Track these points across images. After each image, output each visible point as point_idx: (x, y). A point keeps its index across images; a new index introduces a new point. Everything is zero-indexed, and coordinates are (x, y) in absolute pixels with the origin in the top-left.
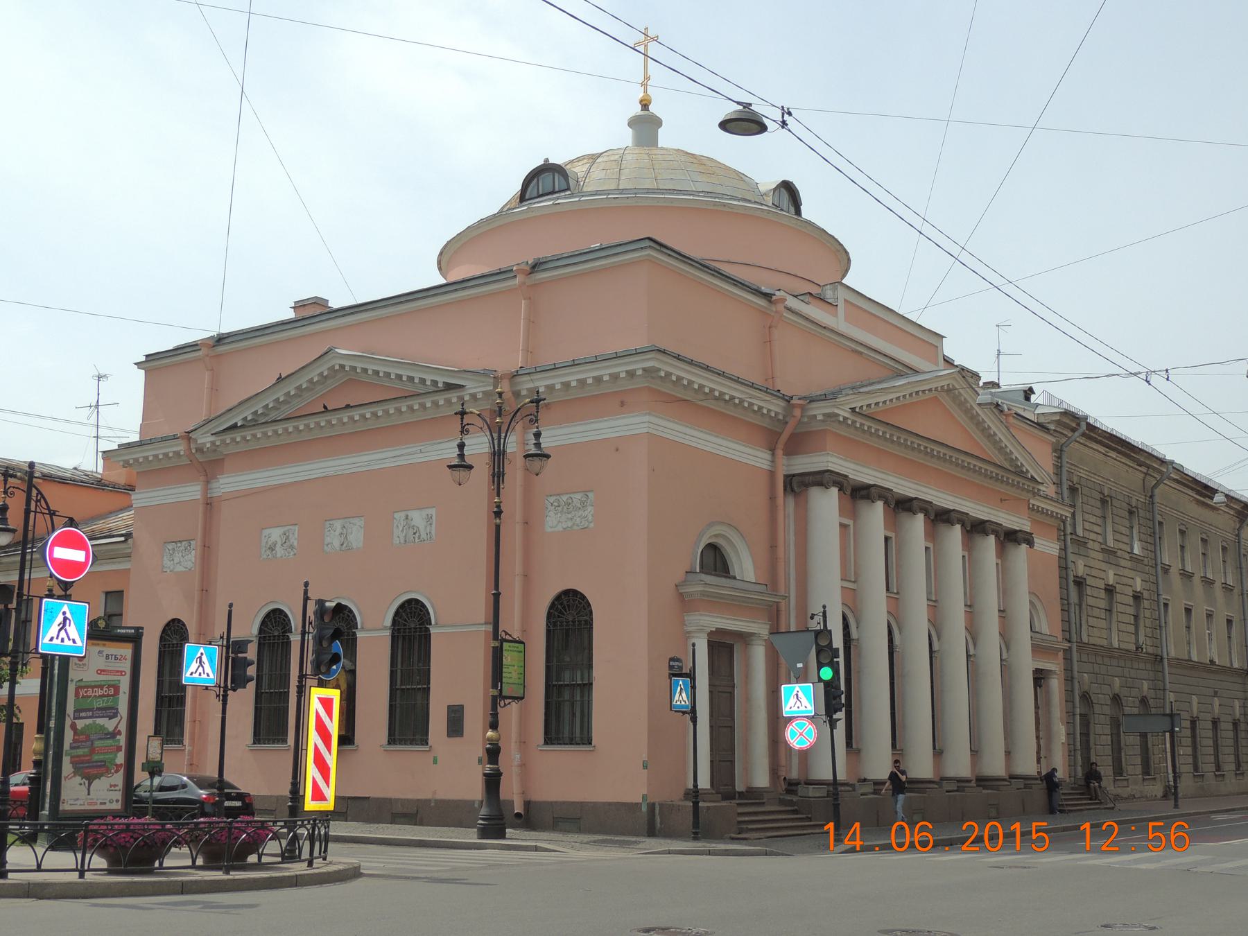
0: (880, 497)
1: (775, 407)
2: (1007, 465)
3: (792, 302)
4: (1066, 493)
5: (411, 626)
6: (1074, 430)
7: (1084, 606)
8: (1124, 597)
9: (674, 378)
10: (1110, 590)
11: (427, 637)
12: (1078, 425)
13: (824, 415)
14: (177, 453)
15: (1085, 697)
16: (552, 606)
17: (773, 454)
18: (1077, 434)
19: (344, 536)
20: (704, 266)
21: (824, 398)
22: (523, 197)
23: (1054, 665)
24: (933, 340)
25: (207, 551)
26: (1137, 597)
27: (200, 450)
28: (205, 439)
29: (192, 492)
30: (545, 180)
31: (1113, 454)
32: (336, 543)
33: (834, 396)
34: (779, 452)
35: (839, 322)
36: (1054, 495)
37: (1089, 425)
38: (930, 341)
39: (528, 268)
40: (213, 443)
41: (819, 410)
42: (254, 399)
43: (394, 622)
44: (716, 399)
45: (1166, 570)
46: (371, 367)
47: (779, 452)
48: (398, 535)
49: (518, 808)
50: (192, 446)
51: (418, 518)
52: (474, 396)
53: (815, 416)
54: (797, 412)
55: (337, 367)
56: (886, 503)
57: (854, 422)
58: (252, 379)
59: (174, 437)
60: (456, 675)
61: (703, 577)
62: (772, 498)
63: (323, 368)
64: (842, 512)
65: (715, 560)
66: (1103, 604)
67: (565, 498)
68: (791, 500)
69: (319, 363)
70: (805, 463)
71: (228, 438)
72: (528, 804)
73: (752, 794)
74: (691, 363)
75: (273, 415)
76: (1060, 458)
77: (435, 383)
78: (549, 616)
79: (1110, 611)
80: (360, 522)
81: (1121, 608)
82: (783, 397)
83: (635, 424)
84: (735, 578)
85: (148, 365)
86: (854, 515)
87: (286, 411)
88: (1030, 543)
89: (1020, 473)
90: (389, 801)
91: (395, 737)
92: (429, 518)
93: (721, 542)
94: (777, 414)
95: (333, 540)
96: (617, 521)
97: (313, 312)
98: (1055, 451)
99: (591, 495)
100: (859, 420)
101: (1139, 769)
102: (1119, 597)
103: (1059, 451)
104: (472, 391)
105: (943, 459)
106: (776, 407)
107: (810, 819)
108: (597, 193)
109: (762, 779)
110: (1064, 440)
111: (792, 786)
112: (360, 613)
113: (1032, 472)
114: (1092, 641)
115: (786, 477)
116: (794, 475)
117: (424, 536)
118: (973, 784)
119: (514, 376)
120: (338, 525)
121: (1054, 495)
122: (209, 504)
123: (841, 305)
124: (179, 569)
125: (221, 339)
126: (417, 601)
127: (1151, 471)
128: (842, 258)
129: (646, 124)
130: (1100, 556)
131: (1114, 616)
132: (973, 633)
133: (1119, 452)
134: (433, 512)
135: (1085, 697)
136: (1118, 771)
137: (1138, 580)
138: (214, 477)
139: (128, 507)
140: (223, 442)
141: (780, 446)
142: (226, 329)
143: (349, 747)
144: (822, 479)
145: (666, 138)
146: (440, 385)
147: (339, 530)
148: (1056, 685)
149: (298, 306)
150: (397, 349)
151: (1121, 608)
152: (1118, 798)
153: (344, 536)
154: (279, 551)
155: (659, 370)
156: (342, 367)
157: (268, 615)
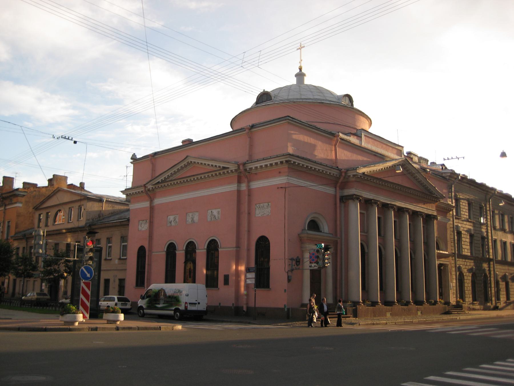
3: (341, 135)
5: (213, 247)
11: (175, 254)
17: (336, 189)
22: (257, 103)
25: (151, 223)
27: (149, 190)
28: (150, 187)
30: (264, 97)
31: (472, 187)
32: (190, 220)
34: (338, 188)
35: (365, 143)
40: (152, 188)
42: (163, 173)
43: (208, 247)
44: (313, 170)
47: (338, 188)
48: (209, 219)
49: (245, 309)
51: (215, 212)
52: (232, 171)
58: (162, 166)
59: (141, 186)
63: (185, 163)
65: (314, 225)
67: (261, 205)
70: (348, 192)
71: (157, 186)
75: (171, 178)
77: (219, 167)
78: (256, 245)
80: (197, 214)
83: (280, 180)
84: (321, 232)
86: (367, 210)
92: (218, 213)
93: (316, 220)
95: (189, 220)
96: (274, 214)
97: (188, 143)
99: (270, 204)
102: (475, 238)
117: (217, 218)
119: (244, 164)
120: (191, 214)
122: (152, 208)
123: (363, 136)
124: (143, 229)
125: (156, 154)
126: (193, 242)
129: (300, 76)
134: (219, 210)
138: (154, 199)
140: (155, 187)
145: (307, 81)
154: (173, 224)
155: (291, 161)
156: (191, 162)
157: (188, 243)
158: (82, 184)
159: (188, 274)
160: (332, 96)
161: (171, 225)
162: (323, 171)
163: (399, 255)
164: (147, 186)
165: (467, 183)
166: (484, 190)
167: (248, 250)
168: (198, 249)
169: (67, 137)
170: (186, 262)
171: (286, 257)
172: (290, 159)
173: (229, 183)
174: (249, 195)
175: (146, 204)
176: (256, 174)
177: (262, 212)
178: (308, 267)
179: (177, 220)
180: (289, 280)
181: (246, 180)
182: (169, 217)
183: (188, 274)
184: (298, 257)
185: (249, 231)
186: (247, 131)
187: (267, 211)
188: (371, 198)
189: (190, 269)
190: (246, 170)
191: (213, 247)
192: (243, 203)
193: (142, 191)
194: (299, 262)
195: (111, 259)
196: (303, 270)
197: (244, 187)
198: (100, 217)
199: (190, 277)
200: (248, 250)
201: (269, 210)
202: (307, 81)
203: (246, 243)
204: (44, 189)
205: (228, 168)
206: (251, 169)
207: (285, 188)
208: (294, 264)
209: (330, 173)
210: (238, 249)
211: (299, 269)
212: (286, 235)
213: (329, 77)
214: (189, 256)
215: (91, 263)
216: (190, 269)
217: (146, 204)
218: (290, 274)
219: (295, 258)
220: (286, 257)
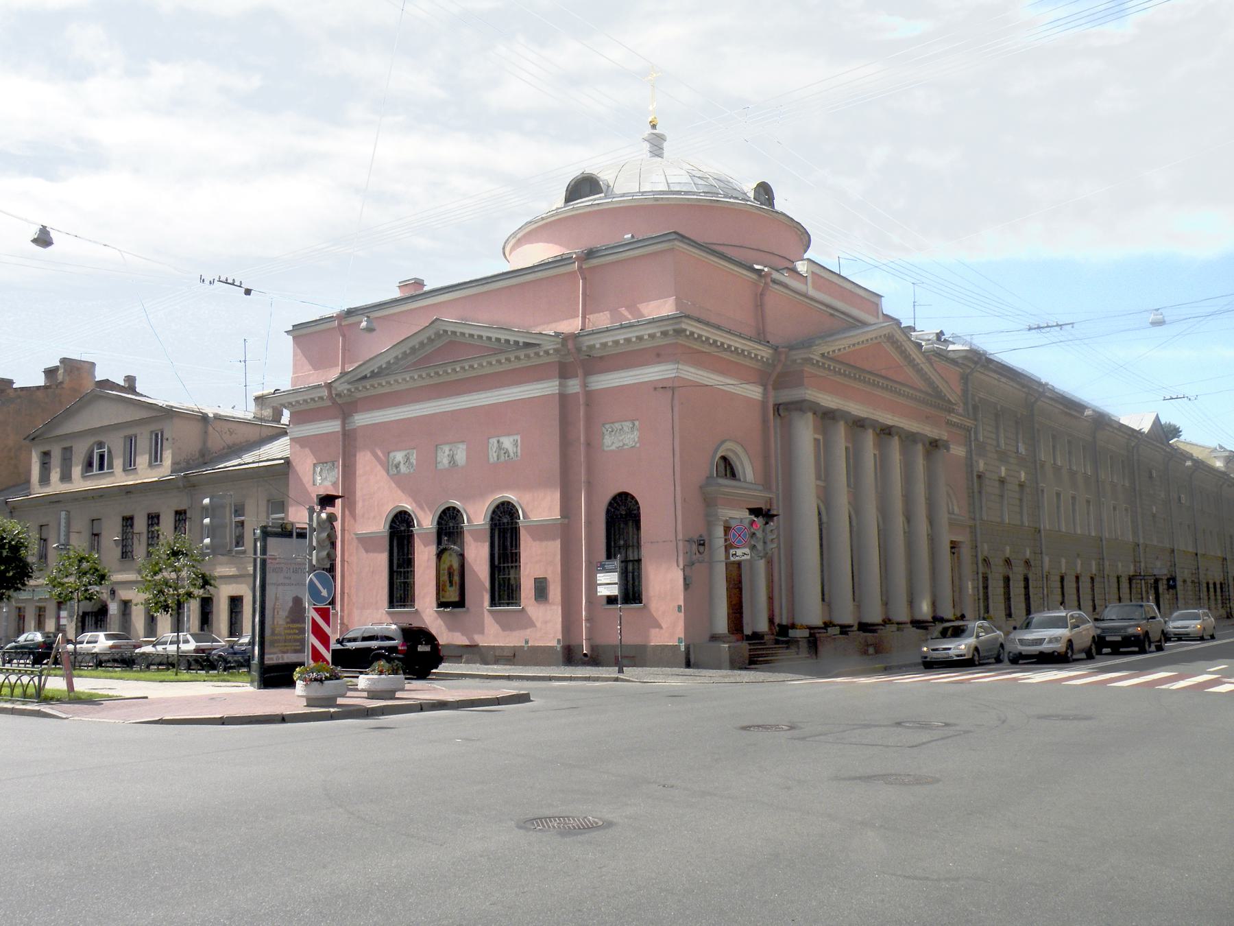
0: (897, 433)
1: (765, 353)
2: (930, 391)
5: (505, 525)
10: (1002, 481)
14: (321, 398)
16: (610, 504)
19: (452, 458)
24: (875, 299)
27: (339, 395)
29: (334, 426)
31: (1003, 380)
32: (446, 461)
33: (807, 343)
38: (872, 300)
40: (349, 390)
41: (799, 355)
45: (1042, 466)
46: (467, 331)
47: (770, 387)
48: (493, 456)
51: (507, 442)
52: (547, 352)
54: (783, 357)
56: (846, 422)
58: (380, 345)
59: (319, 386)
62: (765, 421)
63: (431, 333)
64: (816, 430)
65: (728, 468)
68: (778, 420)
72: (593, 648)
73: (756, 636)
76: (966, 383)
79: (1002, 496)
82: (771, 347)
85: (297, 333)
88: (948, 448)
93: (730, 455)
95: (444, 461)
97: (415, 291)
100: (827, 363)
105: (886, 388)
106: (765, 353)
108: (623, 195)
109: (763, 626)
120: (446, 448)
128: (804, 238)
132: (908, 518)
134: (518, 437)
135: (986, 561)
137: (1023, 475)
138: (350, 415)
140: (357, 389)
144: (800, 406)
147: (447, 452)
148: (966, 552)
149: (403, 286)
150: (485, 320)
153: (452, 458)
154: (403, 469)
156: (445, 332)
158: (131, 380)
159: (445, 578)
161: (399, 472)
163: (824, 519)
165: (995, 372)
166: (1023, 386)
169: (230, 281)
171: (680, 537)
172: (684, 326)
173: (540, 379)
176: (601, 358)
177: (620, 438)
179: (413, 460)
181: (580, 372)
182: (392, 455)
189: (450, 568)
192: (574, 425)
196: (711, 564)
197: (574, 386)
198: (203, 456)
201: (635, 435)
204: (39, 393)
206: (592, 347)
207: (673, 389)
210: (566, 521)
212: (678, 488)
215: (603, 591)
216: (450, 568)
218: (687, 569)
219: (696, 538)
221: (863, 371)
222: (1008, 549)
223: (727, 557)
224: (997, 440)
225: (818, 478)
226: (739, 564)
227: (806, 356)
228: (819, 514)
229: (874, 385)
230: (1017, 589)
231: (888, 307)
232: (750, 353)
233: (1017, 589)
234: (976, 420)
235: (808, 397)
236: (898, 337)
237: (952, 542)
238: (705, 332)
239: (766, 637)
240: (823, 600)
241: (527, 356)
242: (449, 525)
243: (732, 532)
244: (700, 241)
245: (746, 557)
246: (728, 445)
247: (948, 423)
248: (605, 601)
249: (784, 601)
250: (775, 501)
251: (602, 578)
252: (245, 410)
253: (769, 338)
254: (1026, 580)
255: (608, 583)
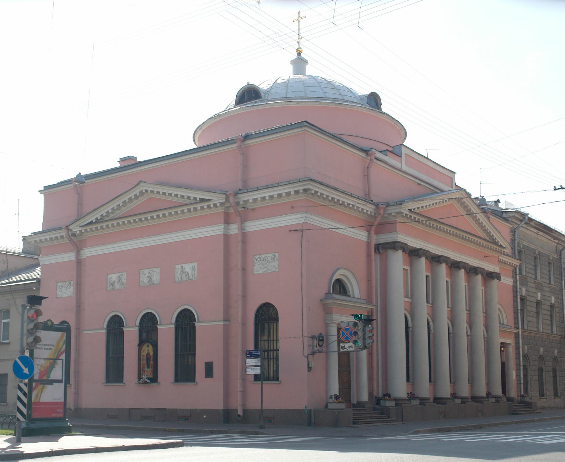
1: (369, 208)
2: (487, 238)
4: (517, 253)
5: (186, 322)
6: (521, 221)
7: (525, 311)
8: (545, 307)
9: (319, 194)
10: (538, 303)
12: (524, 218)
13: (395, 213)
15: (525, 357)
16: (258, 311)
18: (523, 223)
19: (150, 278)
20: (334, 137)
21: (396, 204)
23: (510, 341)
26: (552, 306)
27: (74, 235)
31: (541, 233)
33: (401, 203)
34: (372, 232)
36: (511, 254)
37: (529, 218)
39: (242, 138)
41: (392, 210)
43: (140, 323)
48: (178, 277)
49: (240, 413)
50: (70, 233)
52: (215, 205)
53: (391, 214)
54: (382, 211)
55: (144, 191)
57: (411, 216)
60: (206, 349)
61: (335, 296)
62: (369, 256)
63: (137, 191)
65: (340, 287)
66: (534, 310)
67: (263, 256)
68: (378, 256)
69: (112, 202)
70: (385, 238)
71: (88, 228)
72: (244, 411)
73: (360, 404)
74: (328, 186)
75: (112, 216)
76: (514, 235)
77: (195, 198)
78: (256, 316)
79: (538, 313)
80: (158, 270)
81: (544, 312)
82: (374, 204)
84: (350, 296)
85: (46, 191)
87: (118, 213)
88: (499, 278)
89: (496, 243)
90: (175, 411)
91: (177, 379)
92: (193, 269)
94: (371, 212)
95: (144, 280)
97: (129, 164)
98: (512, 232)
100: (413, 216)
101: (552, 394)
102: (544, 307)
103: (513, 232)
104: (215, 203)
106: (369, 208)
107: (389, 417)
108: (276, 99)
110: (516, 226)
111: (378, 401)
112: (159, 316)
113: (501, 243)
114: (529, 328)
115: (376, 245)
116: (380, 244)
117: (191, 277)
118: (470, 400)
120: (146, 271)
121: (511, 254)
122: (79, 263)
124: (65, 295)
127: (560, 242)
128: (402, 132)
129: (300, 63)
130: (534, 285)
131: (540, 317)
132: (471, 324)
133: (544, 232)
134: (195, 264)
136: (542, 395)
137: (553, 299)
138: (82, 249)
139: (38, 265)
140: (86, 230)
141: (373, 228)
142: (86, 171)
143: (155, 384)
144: (395, 246)
145: (311, 70)
146: (198, 199)
148: (511, 350)
149: (122, 160)
151: (544, 312)
152: (543, 408)
153: (150, 278)
154: (117, 286)
156: (147, 191)
159: (144, 362)
160: (351, 95)
162: (353, 206)
164: (70, 227)
165: (535, 228)
167: (244, 324)
168: (161, 324)
170: (141, 344)
172: (310, 187)
174: (244, 242)
175: (70, 256)
176: (253, 209)
177: (264, 265)
178: (336, 349)
179: (124, 280)
180: (310, 369)
182: (109, 276)
183: (145, 362)
184: (321, 334)
185: (244, 296)
186: (239, 143)
187: (274, 266)
188: (418, 247)
189: (148, 354)
190: (238, 203)
191: (186, 322)
192: (234, 254)
193: (62, 237)
194: (322, 340)
195: (9, 343)
196: (327, 353)
197: (234, 229)
199: (148, 367)
200: (244, 324)
201: (276, 264)
202: (311, 70)
203: (240, 314)
205: (210, 200)
206: (246, 202)
207: (302, 231)
208: (315, 345)
209: (363, 209)
210: (227, 323)
211: (322, 352)
213: (346, 67)
214: (144, 335)
215: (251, 371)
216: (148, 354)
217: (70, 256)
219: (317, 334)
220: (305, 334)
221: (431, 219)
222: (542, 349)
223: (339, 349)
224: (536, 274)
225: (406, 296)
226: (348, 353)
227: (398, 211)
228: (406, 321)
229: (447, 232)
230: (548, 377)
231: (460, 181)
232: (353, 206)
233: (548, 377)
234: (520, 260)
235: (399, 239)
236: (434, 181)
237: (501, 343)
238: (326, 192)
239: (366, 406)
240: (408, 380)
241: (202, 208)
242: (149, 324)
243: (341, 332)
244: (332, 132)
245: (351, 349)
246: (341, 271)
247: (500, 262)
248: (252, 378)
249: (380, 381)
250: (375, 311)
251: (251, 362)
252: (17, 247)
253: (373, 198)
254: (554, 371)
255: (253, 366)
